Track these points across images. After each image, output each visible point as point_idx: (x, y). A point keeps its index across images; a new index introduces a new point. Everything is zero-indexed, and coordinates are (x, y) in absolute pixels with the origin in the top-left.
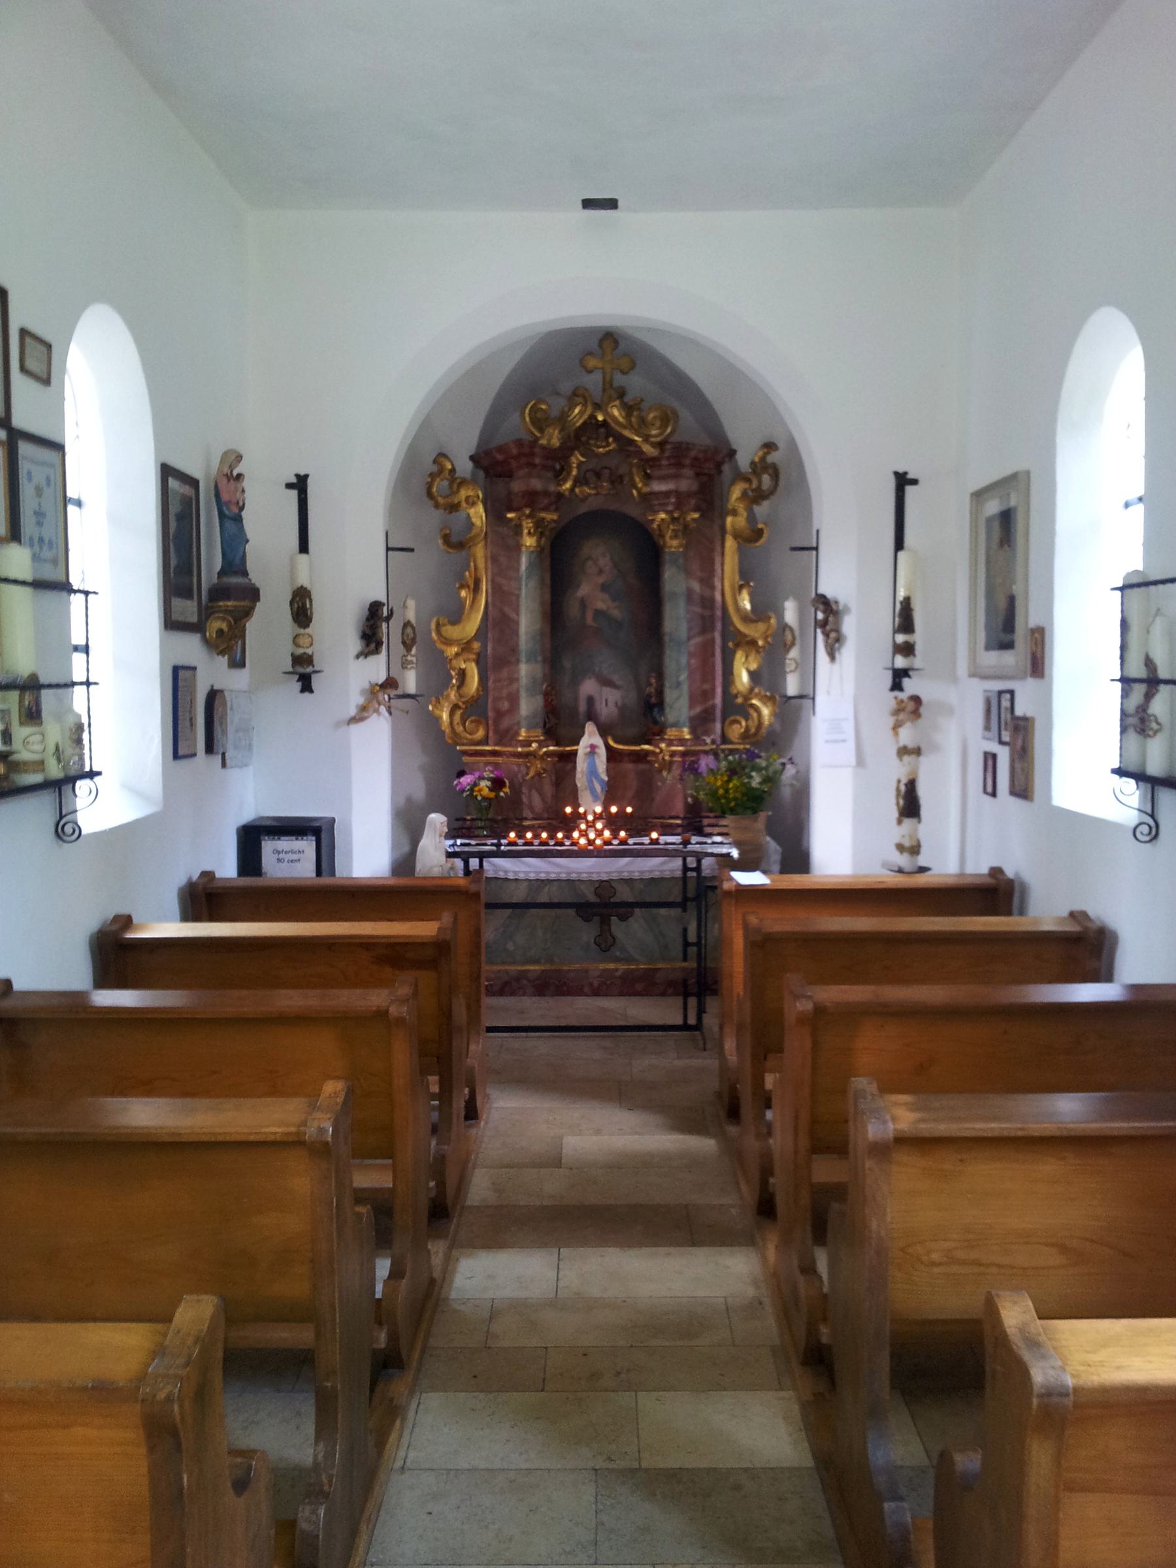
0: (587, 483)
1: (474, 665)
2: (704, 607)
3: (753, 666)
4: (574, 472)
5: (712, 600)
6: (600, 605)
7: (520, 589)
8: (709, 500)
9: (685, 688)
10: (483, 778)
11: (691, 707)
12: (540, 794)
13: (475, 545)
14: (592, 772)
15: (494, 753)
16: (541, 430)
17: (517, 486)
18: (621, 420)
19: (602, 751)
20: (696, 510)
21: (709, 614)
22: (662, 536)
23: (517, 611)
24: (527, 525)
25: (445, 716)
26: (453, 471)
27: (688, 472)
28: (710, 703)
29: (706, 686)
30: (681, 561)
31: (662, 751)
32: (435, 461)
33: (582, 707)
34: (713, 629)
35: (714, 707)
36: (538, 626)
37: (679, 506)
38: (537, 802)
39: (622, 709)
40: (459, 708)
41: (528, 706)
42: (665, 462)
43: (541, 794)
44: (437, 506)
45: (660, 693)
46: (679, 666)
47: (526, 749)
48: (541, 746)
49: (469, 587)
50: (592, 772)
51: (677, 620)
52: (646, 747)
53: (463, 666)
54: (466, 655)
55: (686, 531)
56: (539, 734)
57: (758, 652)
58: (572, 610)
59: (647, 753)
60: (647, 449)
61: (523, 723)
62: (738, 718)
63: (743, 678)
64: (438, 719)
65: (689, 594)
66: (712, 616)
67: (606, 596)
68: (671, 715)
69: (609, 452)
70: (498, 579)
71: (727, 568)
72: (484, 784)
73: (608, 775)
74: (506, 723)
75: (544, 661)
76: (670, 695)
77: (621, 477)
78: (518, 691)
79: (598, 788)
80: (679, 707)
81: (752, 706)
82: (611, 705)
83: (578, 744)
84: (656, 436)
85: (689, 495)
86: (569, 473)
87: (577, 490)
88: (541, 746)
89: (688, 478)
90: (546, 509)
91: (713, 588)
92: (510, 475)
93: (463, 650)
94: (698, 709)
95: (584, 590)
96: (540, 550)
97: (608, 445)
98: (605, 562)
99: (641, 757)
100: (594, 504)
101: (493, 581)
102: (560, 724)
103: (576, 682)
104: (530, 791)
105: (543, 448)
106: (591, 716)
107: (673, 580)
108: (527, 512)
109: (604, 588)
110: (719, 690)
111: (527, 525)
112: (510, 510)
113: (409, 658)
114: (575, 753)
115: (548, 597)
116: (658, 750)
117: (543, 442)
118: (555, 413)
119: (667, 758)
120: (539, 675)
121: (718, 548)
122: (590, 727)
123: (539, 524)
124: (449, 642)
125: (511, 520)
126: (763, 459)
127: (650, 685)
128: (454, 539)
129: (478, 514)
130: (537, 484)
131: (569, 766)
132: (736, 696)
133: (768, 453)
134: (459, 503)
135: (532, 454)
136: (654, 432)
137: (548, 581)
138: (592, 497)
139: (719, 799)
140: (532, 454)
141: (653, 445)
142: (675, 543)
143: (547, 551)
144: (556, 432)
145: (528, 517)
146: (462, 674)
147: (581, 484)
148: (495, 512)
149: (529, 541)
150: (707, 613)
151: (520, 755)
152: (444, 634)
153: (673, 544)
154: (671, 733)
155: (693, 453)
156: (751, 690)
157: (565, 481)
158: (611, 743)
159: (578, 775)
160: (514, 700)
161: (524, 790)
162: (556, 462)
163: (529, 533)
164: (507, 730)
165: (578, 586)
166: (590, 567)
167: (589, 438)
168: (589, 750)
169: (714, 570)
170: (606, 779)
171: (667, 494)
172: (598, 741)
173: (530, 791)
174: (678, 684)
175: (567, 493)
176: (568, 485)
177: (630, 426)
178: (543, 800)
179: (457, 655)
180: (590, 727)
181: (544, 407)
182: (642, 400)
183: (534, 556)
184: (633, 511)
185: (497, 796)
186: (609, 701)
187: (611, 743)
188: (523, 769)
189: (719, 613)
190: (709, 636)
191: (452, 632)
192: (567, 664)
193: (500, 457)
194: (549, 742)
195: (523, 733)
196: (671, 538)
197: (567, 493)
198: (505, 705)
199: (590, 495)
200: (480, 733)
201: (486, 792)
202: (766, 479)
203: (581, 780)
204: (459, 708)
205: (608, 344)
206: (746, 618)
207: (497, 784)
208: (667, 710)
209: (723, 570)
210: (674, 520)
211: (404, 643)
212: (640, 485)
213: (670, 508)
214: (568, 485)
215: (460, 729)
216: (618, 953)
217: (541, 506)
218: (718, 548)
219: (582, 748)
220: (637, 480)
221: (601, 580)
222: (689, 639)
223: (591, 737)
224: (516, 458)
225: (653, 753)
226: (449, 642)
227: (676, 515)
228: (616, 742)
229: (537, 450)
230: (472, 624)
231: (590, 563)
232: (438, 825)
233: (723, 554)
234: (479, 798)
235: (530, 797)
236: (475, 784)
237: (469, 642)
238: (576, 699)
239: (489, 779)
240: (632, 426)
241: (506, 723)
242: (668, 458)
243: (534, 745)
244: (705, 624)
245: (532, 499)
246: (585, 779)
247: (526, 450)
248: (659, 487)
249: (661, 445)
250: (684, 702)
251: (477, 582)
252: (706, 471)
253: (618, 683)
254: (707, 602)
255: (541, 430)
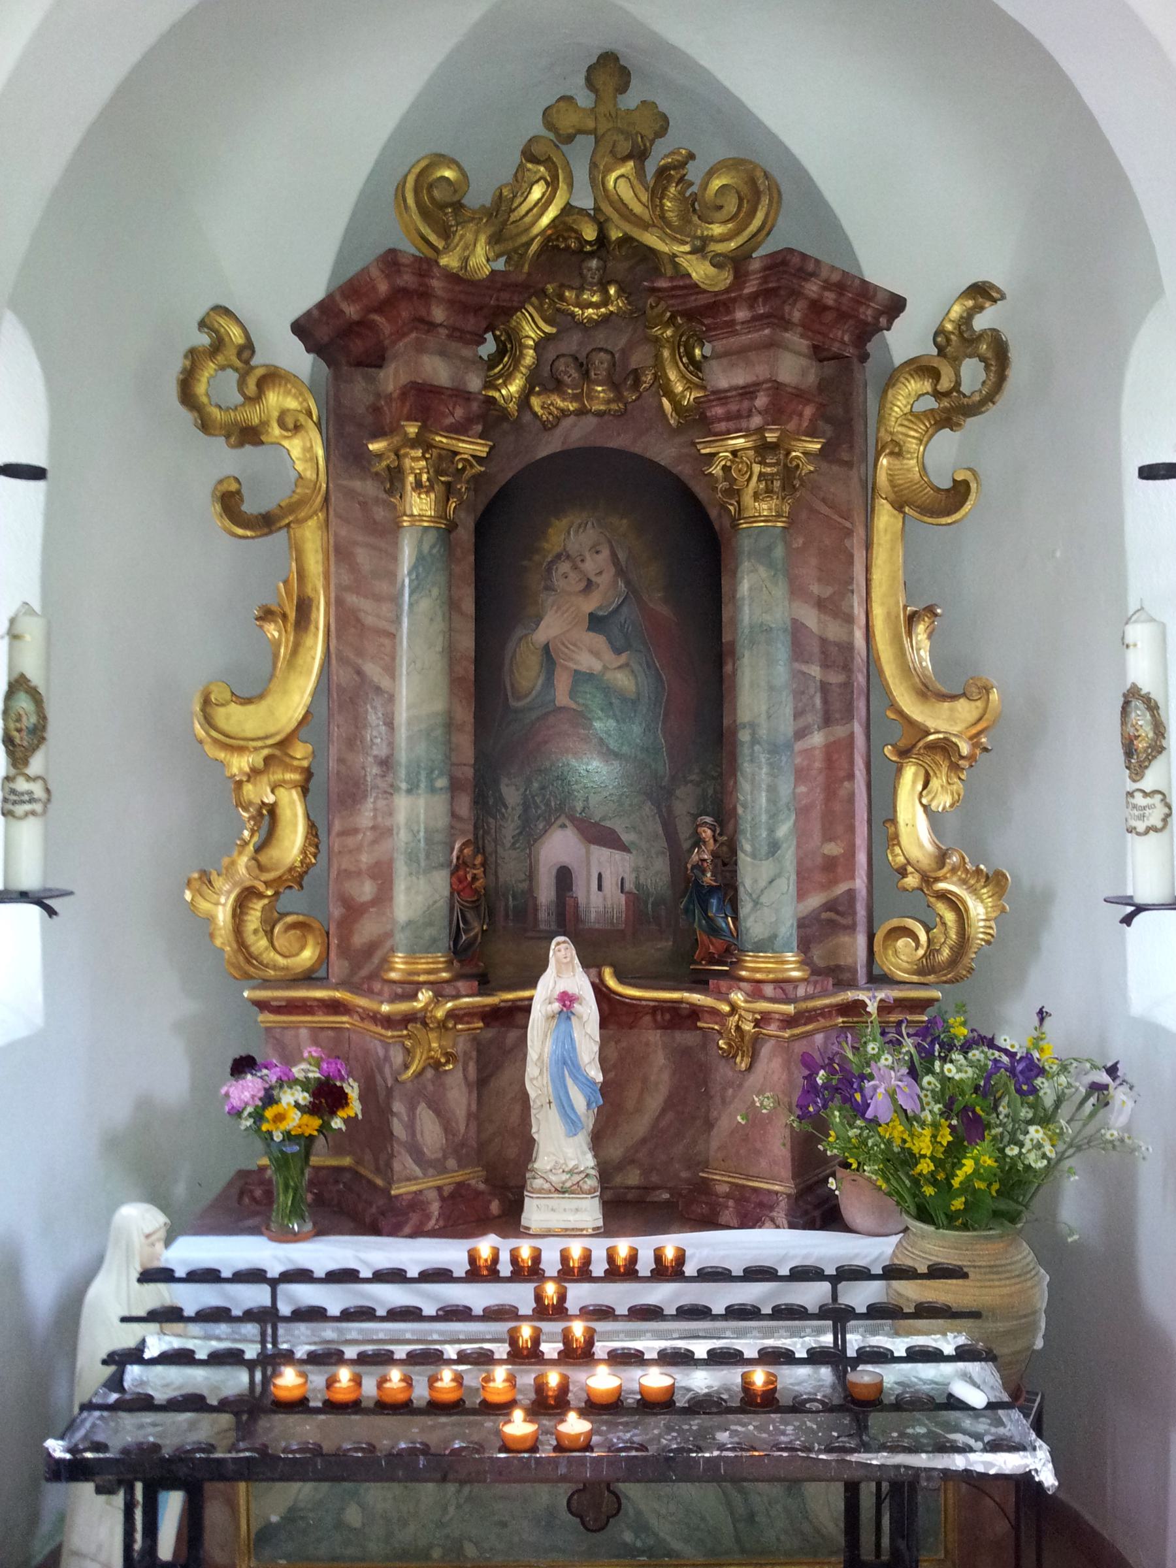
0: (557, 385)
1: (295, 795)
2: (826, 665)
3: (942, 801)
4: (529, 357)
5: (847, 648)
6: (586, 662)
7: (397, 620)
8: (838, 408)
9: (789, 856)
10: (293, 1082)
11: (801, 895)
12: (438, 1112)
13: (300, 522)
14: (567, 1062)
15: (335, 1007)
16: (446, 233)
17: (392, 378)
18: (638, 209)
19: (589, 1009)
20: (812, 433)
21: (841, 683)
22: (734, 493)
23: (391, 670)
24: (416, 464)
25: (223, 915)
26: (248, 348)
27: (796, 340)
28: (841, 889)
29: (833, 849)
30: (779, 552)
31: (734, 1009)
32: (203, 324)
33: (546, 893)
34: (848, 714)
35: (851, 894)
36: (439, 705)
37: (776, 413)
38: (430, 1132)
39: (636, 900)
40: (261, 896)
41: (416, 897)
42: (741, 314)
43: (438, 1108)
44: (205, 425)
45: (727, 861)
46: (768, 797)
47: (403, 1007)
48: (439, 995)
49: (284, 616)
50: (567, 1062)
51: (765, 692)
52: (696, 998)
53: (270, 799)
54: (278, 775)
55: (788, 480)
56: (434, 964)
57: (955, 767)
58: (526, 674)
59: (695, 1013)
60: (699, 271)
61: (401, 938)
62: (910, 923)
63: (915, 834)
64: (210, 919)
65: (797, 630)
66: (848, 685)
67: (599, 641)
68: (755, 924)
69: (606, 319)
70: (352, 599)
71: (879, 576)
72: (292, 1097)
73: (604, 1071)
74: (366, 931)
75: (455, 786)
76: (753, 873)
77: (636, 375)
78: (390, 863)
79: (579, 1100)
80: (772, 901)
81: (943, 896)
82: (610, 883)
83: (533, 984)
84: (723, 239)
85: (800, 395)
86: (517, 361)
87: (535, 402)
88: (439, 995)
89: (799, 354)
90: (460, 429)
91: (849, 619)
92: (376, 359)
93: (268, 760)
94: (815, 901)
95: (551, 627)
96: (447, 529)
97: (606, 301)
98: (597, 564)
99: (681, 1018)
100: (575, 433)
101: (339, 602)
102: (491, 935)
103: (530, 836)
104: (412, 1109)
105: (453, 278)
106: (567, 919)
107: (760, 598)
108: (412, 429)
109: (596, 622)
110: (862, 858)
111: (416, 464)
112: (376, 436)
113: (22, 785)
114: (525, 1009)
115: (467, 643)
116: (726, 1008)
117: (449, 261)
118: (479, 196)
119: (748, 1027)
120: (442, 821)
121: (860, 531)
122: (561, 951)
123: (443, 462)
124: (233, 744)
125: (379, 456)
126: (966, 321)
127: (698, 842)
128: (250, 507)
129: (303, 453)
130: (437, 370)
131: (512, 1035)
132: (902, 872)
133: (980, 308)
134: (265, 424)
135: (424, 295)
136: (717, 230)
137: (469, 606)
138: (571, 418)
139: (916, 1182)
140: (424, 295)
141: (718, 262)
142: (765, 508)
143: (465, 534)
144: (483, 239)
145: (414, 443)
146: (269, 816)
147: (546, 390)
148: (346, 435)
149: (421, 504)
150: (835, 678)
151: (388, 1021)
152: (221, 722)
153: (761, 509)
154: (756, 965)
155: (812, 288)
156: (942, 857)
157: (508, 377)
158: (612, 983)
159: (532, 1070)
160: (383, 875)
161: (398, 1106)
162: (484, 310)
163: (418, 485)
164: (371, 948)
165: (538, 619)
166: (565, 577)
167: (562, 286)
168: (556, 1006)
169: (851, 580)
170: (600, 1078)
171: (748, 392)
172: (580, 983)
173: (412, 1109)
174: (774, 847)
175: (512, 407)
176: (514, 387)
177: (661, 221)
178: (447, 1129)
179: (254, 773)
180: (561, 951)
181: (448, 174)
182: (691, 156)
183: (431, 537)
184: (664, 452)
185: (324, 1128)
186: (607, 879)
187: (612, 983)
188: (398, 1057)
189: (860, 679)
190: (840, 731)
191: (240, 719)
192: (511, 794)
193: (351, 311)
194: (461, 985)
195: (399, 966)
196: (756, 497)
197: (512, 407)
198: (366, 890)
199: (565, 413)
200: (308, 955)
201: (294, 1120)
202: (972, 374)
203: (537, 1078)
204: (261, 896)
205: (605, 81)
206: (926, 692)
207: (326, 1097)
208: (745, 909)
209: (868, 581)
210: (764, 449)
211: (9, 741)
212: (679, 388)
213: (756, 421)
214: (514, 387)
215: (259, 944)
216: (628, 1537)
217: (450, 420)
218: (860, 531)
219: (542, 997)
220: (672, 375)
221: (590, 605)
222: (800, 734)
223: (564, 975)
224: (384, 306)
225: (714, 1012)
226: (233, 744)
227: (771, 437)
228: (621, 978)
229: (436, 284)
230: (293, 700)
231: (565, 567)
232: (138, 1241)
233: (868, 546)
234: (278, 1137)
235: (411, 1127)
236: (269, 1099)
237: (284, 744)
238: (531, 876)
239: (305, 1085)
240: (668, 224)
241: (366, 931)
242: (752, 299)
243: (424, 996)
244: (835, 705)
245: (424, 400)
246: (546, 1078)
247: (407, 279)
248: (725, 378)
249: (737, 262)
250: (787, 885)
251: (304, 608)
252: (835, 348)
253: (626, 838)
254: (837, 656)
255: (446, 233)
